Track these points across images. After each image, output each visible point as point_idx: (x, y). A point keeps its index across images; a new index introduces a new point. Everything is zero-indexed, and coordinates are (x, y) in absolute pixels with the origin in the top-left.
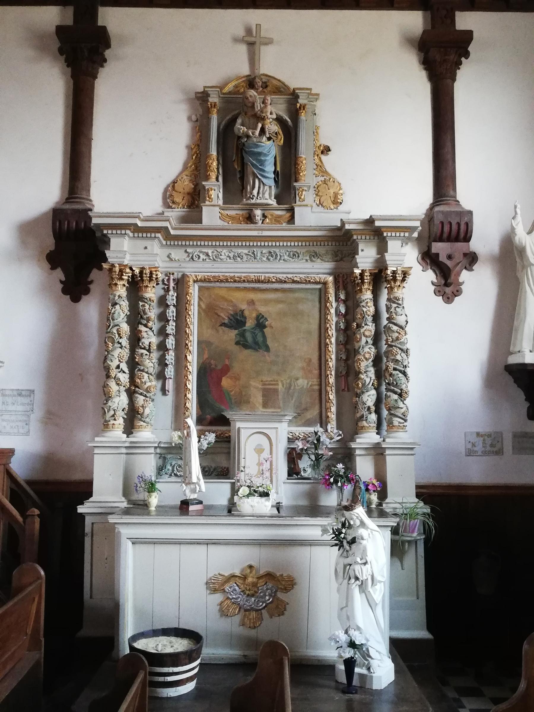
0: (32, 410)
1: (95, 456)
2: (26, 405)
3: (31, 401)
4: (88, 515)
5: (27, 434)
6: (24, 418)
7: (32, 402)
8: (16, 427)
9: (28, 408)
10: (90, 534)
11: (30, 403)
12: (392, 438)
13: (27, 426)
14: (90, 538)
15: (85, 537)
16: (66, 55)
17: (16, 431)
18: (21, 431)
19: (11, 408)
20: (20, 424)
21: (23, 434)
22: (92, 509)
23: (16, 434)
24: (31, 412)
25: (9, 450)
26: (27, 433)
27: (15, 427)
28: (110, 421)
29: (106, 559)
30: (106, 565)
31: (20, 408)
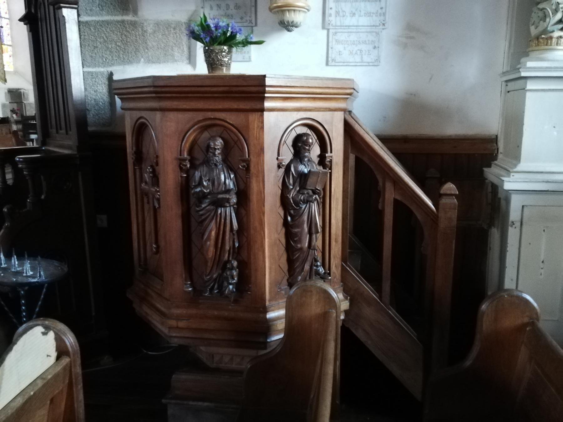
0: (384, 24)
1: (528, 94)
2: (374, 16)
3: (382, 8)
4: (513, 193)
5: (376, 64)
6: (371, 38)
7: (384, 10)
8: (359, 52)
9: (376, 20)
10: (519, 224)
11: (380, 11)
12: (548, 60)
13: (376, 51)
14: (518, 229)
15: (510, 228)
16: (32, 13)
17: (358, 59)
18: (366, 58)
19: (349, 21)
20: (364, 47)
21: (368, 64)
22: (530, 184)
23: (359, 64)
24: (381, 27)
25: (150, 80)
26: (376, 63)
27: (356, 53)
28: (553, 31)
29: (543, 262)
30: (542, 271)
31: (364, 21)
